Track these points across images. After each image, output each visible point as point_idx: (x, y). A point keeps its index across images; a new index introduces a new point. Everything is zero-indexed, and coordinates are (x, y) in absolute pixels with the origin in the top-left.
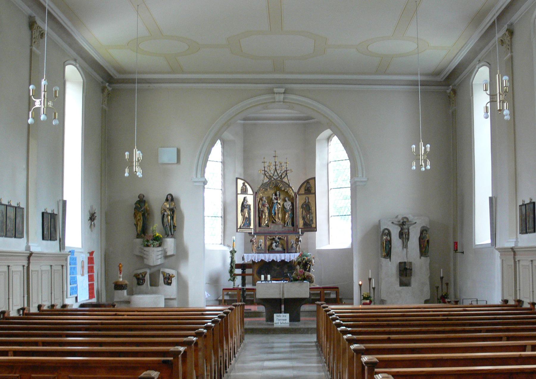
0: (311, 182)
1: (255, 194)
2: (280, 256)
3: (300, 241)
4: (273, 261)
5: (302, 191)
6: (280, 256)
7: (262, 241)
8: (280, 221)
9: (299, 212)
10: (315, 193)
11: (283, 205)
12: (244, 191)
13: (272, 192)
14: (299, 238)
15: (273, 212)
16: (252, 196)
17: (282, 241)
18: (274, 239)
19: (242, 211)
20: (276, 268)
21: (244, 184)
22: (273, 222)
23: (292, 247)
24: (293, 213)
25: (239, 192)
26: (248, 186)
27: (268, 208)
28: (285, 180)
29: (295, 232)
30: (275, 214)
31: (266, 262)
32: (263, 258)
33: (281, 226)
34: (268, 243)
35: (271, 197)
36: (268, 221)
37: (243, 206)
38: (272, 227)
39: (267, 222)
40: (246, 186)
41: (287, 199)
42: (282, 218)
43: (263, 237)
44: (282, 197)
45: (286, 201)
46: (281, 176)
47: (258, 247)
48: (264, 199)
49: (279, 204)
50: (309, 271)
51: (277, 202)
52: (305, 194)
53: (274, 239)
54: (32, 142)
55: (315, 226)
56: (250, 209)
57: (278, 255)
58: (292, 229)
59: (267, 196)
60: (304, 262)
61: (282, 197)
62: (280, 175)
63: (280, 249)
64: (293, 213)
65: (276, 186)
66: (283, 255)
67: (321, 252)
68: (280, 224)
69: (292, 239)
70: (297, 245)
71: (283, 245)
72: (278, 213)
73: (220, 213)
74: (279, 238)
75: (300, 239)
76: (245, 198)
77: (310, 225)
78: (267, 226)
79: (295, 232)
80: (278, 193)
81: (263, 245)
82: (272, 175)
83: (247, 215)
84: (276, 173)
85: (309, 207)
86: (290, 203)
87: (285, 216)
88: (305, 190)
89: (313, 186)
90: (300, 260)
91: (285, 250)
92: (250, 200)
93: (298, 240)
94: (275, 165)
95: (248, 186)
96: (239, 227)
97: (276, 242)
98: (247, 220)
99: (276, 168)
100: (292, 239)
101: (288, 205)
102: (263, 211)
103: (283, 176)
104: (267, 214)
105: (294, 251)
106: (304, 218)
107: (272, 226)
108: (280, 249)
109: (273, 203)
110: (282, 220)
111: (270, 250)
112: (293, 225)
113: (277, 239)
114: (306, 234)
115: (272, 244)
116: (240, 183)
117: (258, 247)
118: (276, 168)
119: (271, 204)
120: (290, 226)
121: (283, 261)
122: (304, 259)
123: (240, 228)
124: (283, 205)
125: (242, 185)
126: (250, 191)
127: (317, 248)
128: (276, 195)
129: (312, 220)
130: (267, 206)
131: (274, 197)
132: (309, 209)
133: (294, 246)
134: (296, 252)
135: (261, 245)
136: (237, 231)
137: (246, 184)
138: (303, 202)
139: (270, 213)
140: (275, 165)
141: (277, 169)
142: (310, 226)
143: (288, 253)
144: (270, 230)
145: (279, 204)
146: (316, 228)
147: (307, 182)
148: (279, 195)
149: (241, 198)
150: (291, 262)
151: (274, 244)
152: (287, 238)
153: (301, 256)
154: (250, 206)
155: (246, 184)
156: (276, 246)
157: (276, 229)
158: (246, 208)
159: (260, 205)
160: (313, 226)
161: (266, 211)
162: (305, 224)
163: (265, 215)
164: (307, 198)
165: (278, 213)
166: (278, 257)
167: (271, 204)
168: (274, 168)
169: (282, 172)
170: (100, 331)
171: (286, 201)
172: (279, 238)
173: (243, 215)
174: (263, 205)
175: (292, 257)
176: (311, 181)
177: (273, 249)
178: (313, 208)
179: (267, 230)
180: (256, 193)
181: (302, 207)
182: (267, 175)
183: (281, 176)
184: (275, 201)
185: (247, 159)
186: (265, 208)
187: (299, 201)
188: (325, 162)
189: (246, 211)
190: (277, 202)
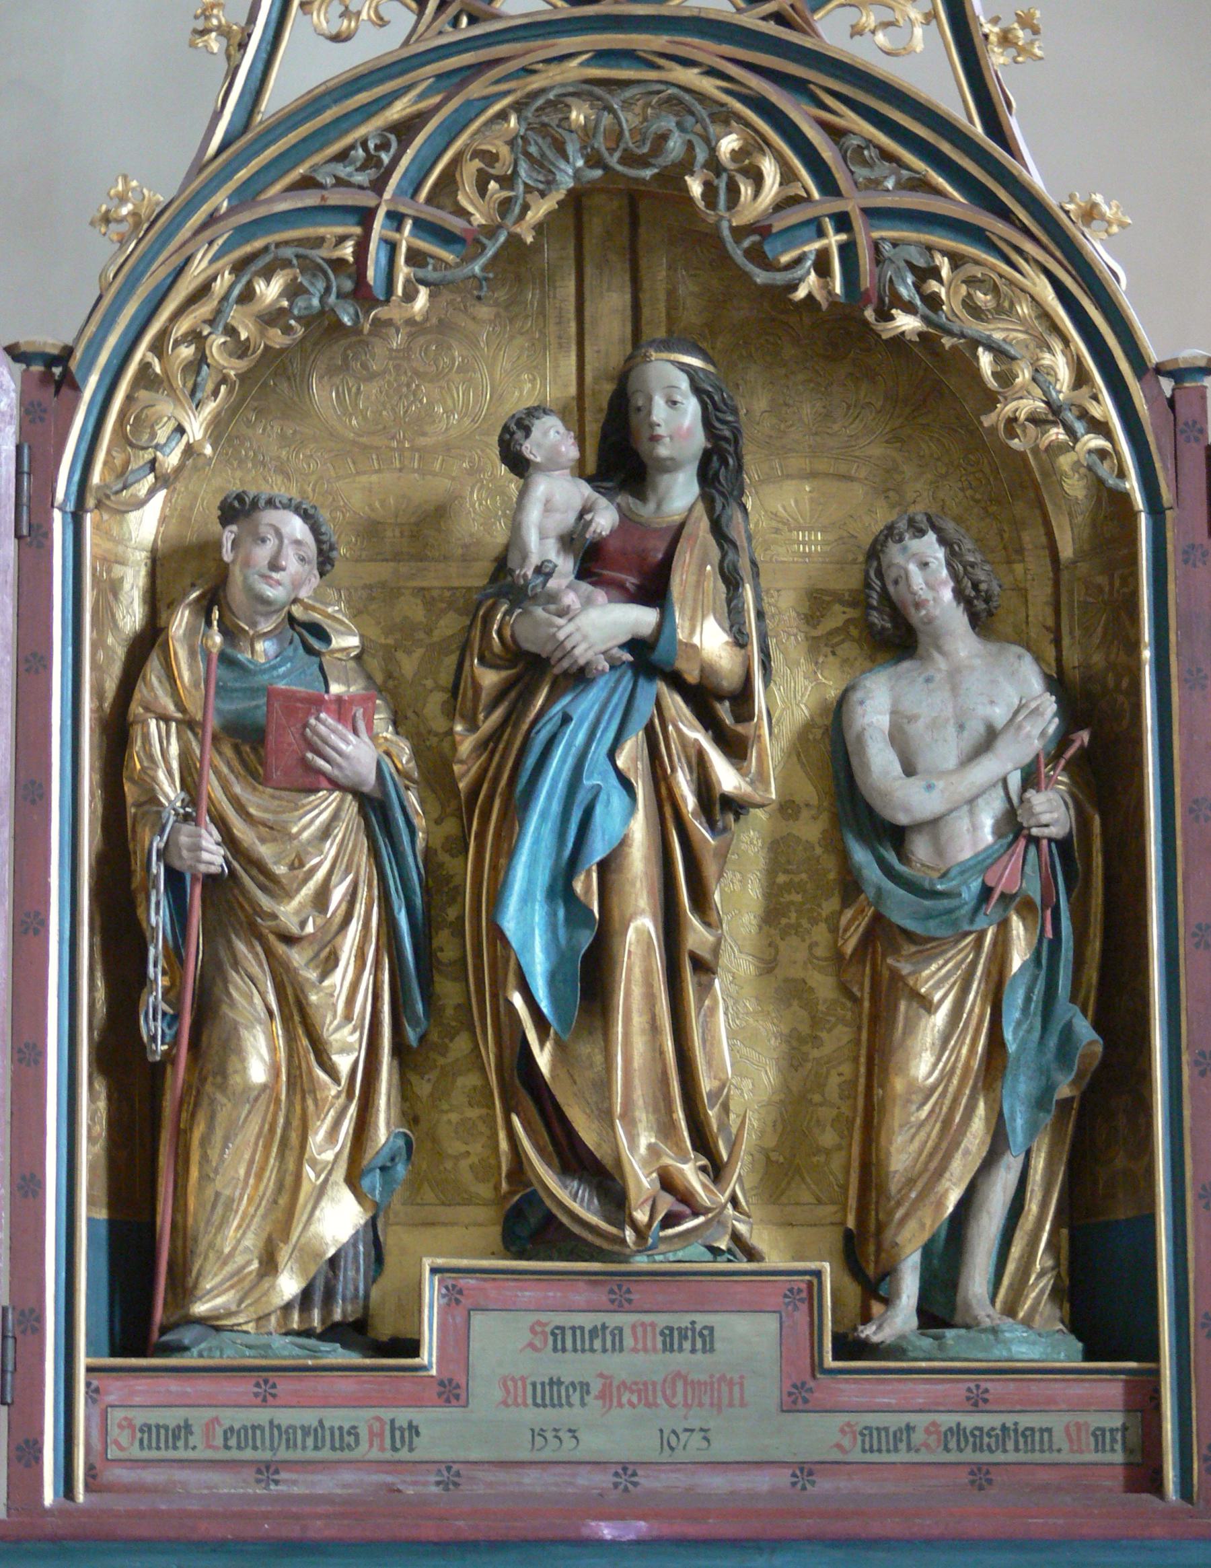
8: (737, 1205)
11: (831, 746)
13: (531, 375)
15: (529, 927)
22: (530, 1229)
33: (750, 1337)
36: (399, 1181)
39: (338, 1219)
41: (927, 574)
42: (794, 1112)
44: (794, 519)
45: (893, 635)
48: (282, 562)
49: (722, 707)
54: (589, 270)
59: (361, 491)
61: (794, 519)
78: (359, 1325)
80: (676, 419)
86: (1011, 694)
87: (877, 1053)
101: (965, 742)
102: (230, 902)
104: (347, 994)
107: (503, 1342)
109: (538, 672)
110: (782, 1172)
120: (1035, 1338)
124: (831, 746)
128: (620, 459)
130: (362, 748)
131: (558, 498)
144: (439, 1433)
148: (719, 470)
159: (161, 751)
161: (322, 861)
163: (297, 1015)
167: (486, 679)
170: (282, 155)
171: (893, 635)
174: (263, 743)
184: (601, 623)
190: (646, 658)
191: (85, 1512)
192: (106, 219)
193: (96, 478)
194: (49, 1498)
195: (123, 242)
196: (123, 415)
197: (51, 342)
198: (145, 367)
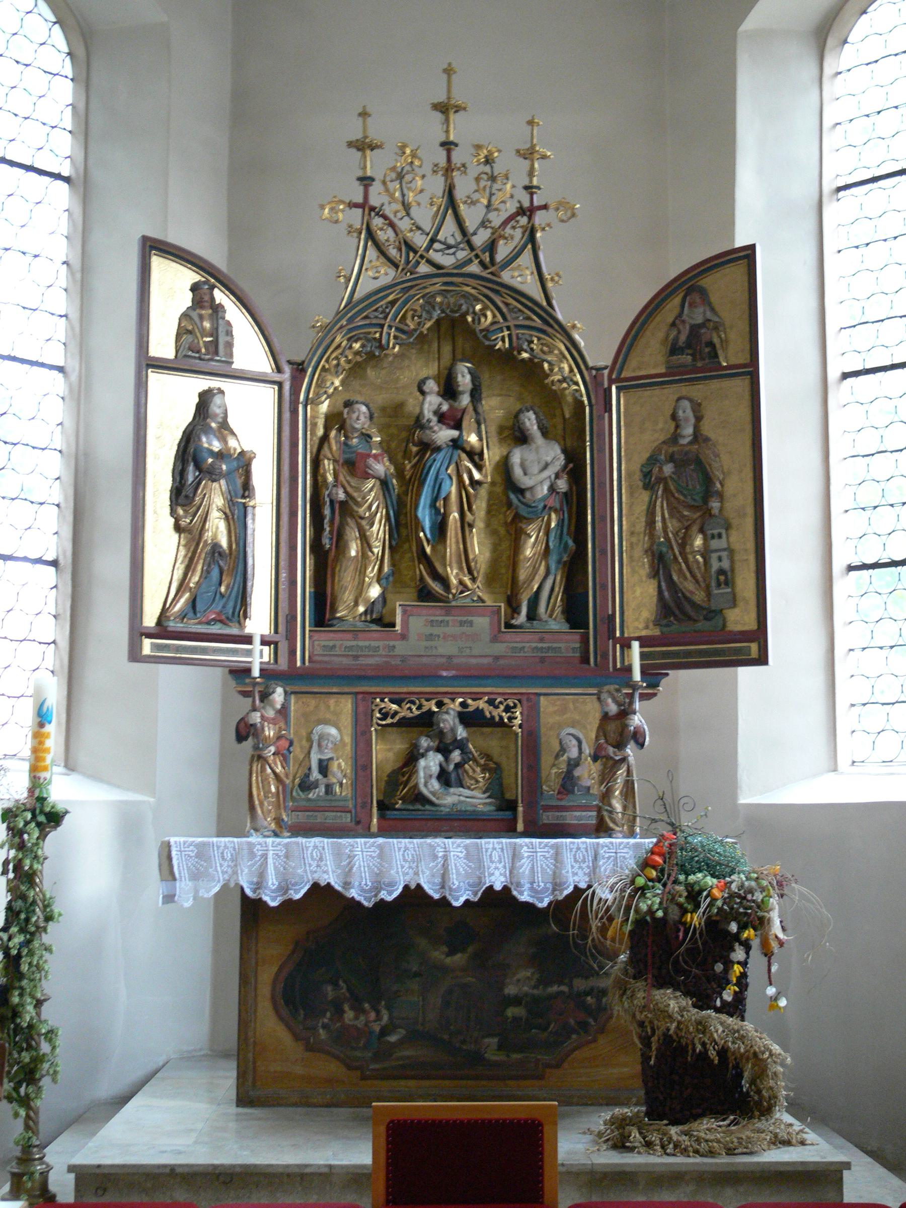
0: (720, 286)
1: (293, 377)
2: (476, 859)
3: (638, 738)
4: (414, 895)
5: (651, 358)
6: (476, 859)
7: (334, 733)
8: (479, 588)
9: (625, 515)
10: (750, 371)
11: (504, 467)
12: (202, 348)
13: (425, 368)
14: (625, 713)
15: (425, 515)
16: (267, 395)
17: (493, 742)
18: (426, 722)
19: (182, 495)
20: (438, 954)
21: (201, 296)
22: (425, 594)
23: (568, 783)
24: (576, 528)
25: (163, 345)
26: (234, 314)
27: (384, 484)
28: (521, 276)
29: (591, 664)
30: (440, 528)
31: (354, 904)
32: (331, 877)
33: (482, 623)
34: (384, 752)
35: (412, 406)
37: (196, 462)
38: (419, 633)
39: (375, 592)
40: (217, 310)
41: (530, 421)
42: (494, 563)
43: (346, 705)
44: (495, 407)
46: (491, 247)
47: (306, 785)
48: (360, 417)
49: (475, 456)
50: (736, 1008)
51: (456, 444)
52: (674, 374)
53: (426, 722)
55: (749, 622)
56: (247, 488)
57: (455, 849)
58: (568, 643)
59: (381, 399)
60: (695, 919)
61: (495, 407)
62: (481, 238)
63: (472, 797)
64: (576, 528)
65: (446, 328)
66: (494, 847)
67: (773, 823)
68: (478, 608)
69: (569, 721)
70: (610, 767)
71: (494, 769)
72: (465, 526)
73: (48, 535)
74: (469, 719)
75: (637, 720)
76: (205, 400)
77: (713, 614)
79: (591, 664)
80: (464, 380)
81: (342, 768)
82: (420, 241)
83: (217, 529)
84: (449, 231)
85: (708, 480)
88: (674, 350)
89: (731, 316)
90: (652, 901)
91: (516, 812)
92: (252, 419)
93: (616, 732)
94: (449, 170)
95: (234, 314)
96: (150, 620)
97: (444, 750)
98: (218, 573)
99: (450, 192)
100: (569, 721)
101: (540, 466)
102: (346, 509)
103: (503, 251)
104: (378, 530)
105: (590, 818)
106: (660, 564)
107: (417, 624)
108: (472, 797)
109: (428, 447)
110: (491, 580)
111: (399, 809)
112: (575, 613)
113: (449, 720)
114: (681, 681)
115: (412, 758)
116: (173, 285)
117: (306, 785)
118: (450, 192)
119: (412, 448)
120: (557, 624)
121: (498, 903)
122: (694, 895)
123: (162, 630)
124: (504, 467)
125: (186, 300)
126: (249, 349)
127: (743, 800)
128: (449, 391)
129: (726, 578)
130: (381, 467)
131: (433, 402)
132: (707, 491)
133: (588, 774)
134: (601, 829)
135: (324, 768)
136: (135, 655)
137: (220, 296)
138: (654, 435)
139: (401, 524)
140: (449, 170)
141: (460, 194)
142: (714, 623)
143: (536, 830)
144: (401, 648)
145: (475, 456)
146: (760, 634)
147: (689, 285)
148: (476, 394)
149: (172, 402)
150: (572, 906)
151: (431, 763)
152: (533, 713)
153: (669, 861)
154: (244, 464)
155: (220, 296)
156: (444, 777)
157: (446, 648)
158: (212, 474)
159: (328, 466)
160: (739, 619)
161: (371, 498)
162: (673, 608)
164: (686, 411)
165: (465, 526)
166: (456, 866)
167: (412, 448)
168: (437, 185)
169: (496, 219)
171: (521, 438)
172: (469, 719)
173: (189, 531)
174: (354, 466)
175: (595, 865)
176: (713, 283)
177: (419, 798)
178: (735, 488)
179: (375, 649)
180: (299, 369)
181: (649, 479)
182: (385, 235)
183: (491, 247)
184: (445, 435)
185: (252, 163)
186: (364, 487)
187: (625, 438)
188: (802, 190)
189: (216, 498)
190: (456, 444)
191: (308, 668)
192: (314, 327)
193: (311, 396)
194: (299, 664)
195: (318, 333)
196: (318, 379)
197: (298, 359)
198: (324, 366)
